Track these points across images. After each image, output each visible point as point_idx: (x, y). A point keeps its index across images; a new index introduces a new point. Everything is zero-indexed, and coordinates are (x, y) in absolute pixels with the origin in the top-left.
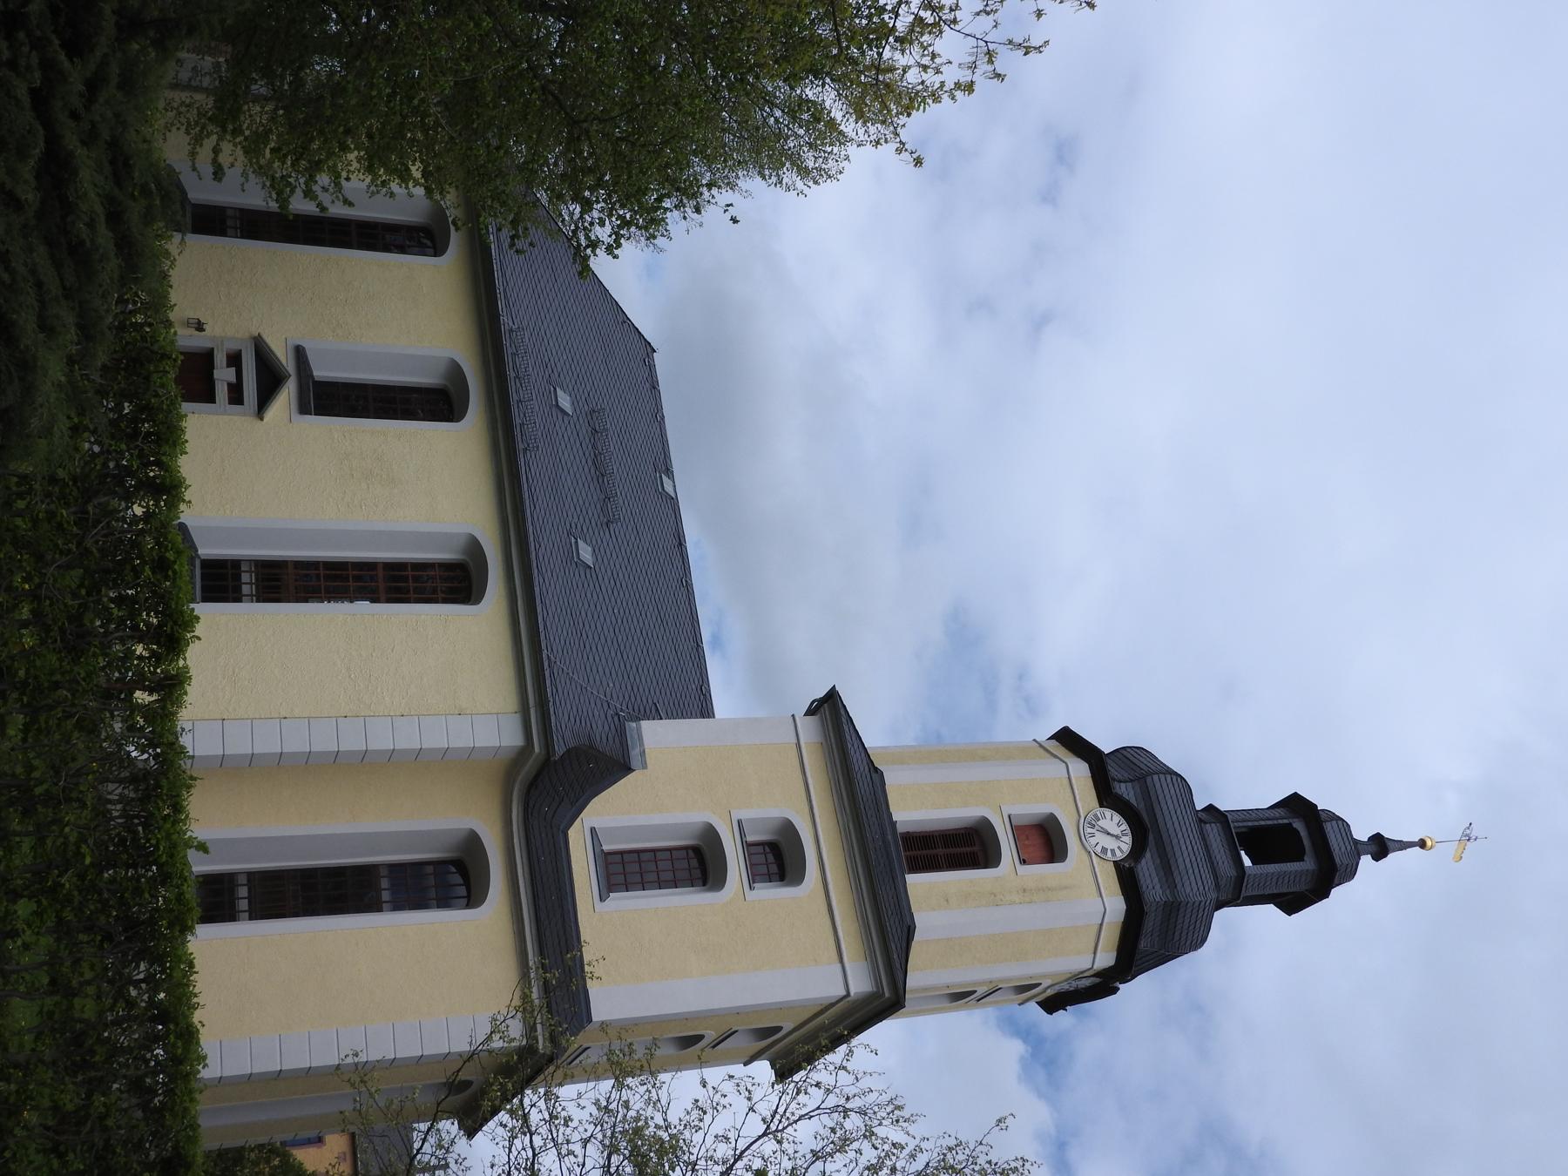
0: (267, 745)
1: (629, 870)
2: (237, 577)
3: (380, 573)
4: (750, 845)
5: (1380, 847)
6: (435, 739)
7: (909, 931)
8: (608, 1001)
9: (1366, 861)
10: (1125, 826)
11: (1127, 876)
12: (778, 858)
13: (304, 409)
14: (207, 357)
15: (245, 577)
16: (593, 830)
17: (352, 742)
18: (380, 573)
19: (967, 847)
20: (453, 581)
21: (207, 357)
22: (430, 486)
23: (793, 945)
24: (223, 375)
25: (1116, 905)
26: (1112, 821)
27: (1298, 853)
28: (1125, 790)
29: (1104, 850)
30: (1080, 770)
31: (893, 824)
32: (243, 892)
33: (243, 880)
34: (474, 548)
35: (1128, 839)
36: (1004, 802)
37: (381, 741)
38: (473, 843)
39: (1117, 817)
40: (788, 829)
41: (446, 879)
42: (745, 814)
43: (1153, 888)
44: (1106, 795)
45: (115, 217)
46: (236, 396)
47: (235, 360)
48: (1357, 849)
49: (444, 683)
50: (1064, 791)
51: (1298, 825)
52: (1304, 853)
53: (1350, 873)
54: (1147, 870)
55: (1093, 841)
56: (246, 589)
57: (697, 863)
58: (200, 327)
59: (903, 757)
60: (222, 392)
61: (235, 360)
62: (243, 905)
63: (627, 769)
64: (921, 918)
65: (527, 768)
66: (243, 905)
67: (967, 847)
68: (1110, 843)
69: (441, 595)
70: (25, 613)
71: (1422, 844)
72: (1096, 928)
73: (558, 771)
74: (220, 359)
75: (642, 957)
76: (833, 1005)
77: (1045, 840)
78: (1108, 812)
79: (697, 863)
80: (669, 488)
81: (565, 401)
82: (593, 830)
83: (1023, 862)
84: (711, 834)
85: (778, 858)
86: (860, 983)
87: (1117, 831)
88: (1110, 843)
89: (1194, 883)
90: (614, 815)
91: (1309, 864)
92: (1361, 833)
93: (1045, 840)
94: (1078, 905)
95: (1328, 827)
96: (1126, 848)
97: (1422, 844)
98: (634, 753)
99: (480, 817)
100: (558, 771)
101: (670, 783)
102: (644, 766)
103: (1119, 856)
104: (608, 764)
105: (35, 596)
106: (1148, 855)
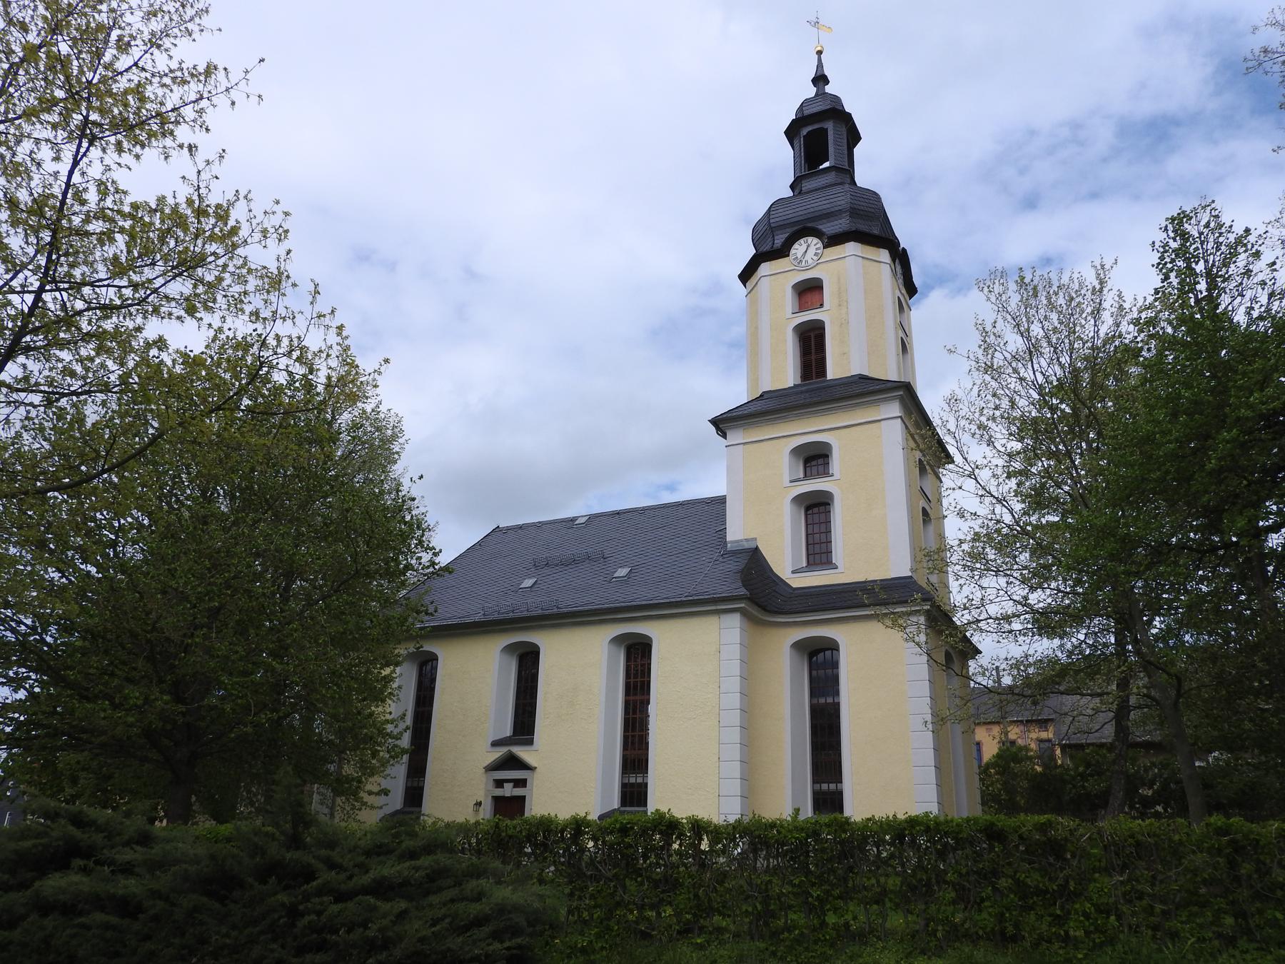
0: (735, 769)
1: (818, 550)
5: (820, 79)
6: (735, 667)
7: (863, 378)
8: (898, 565)
10: (802, 241)
11: (833, 241)
12: (814, 458)
15: (632, 780)
16: (793, 572)
17: (735, 718)
18: (631, 698)
19: (811, 341)
20: (638, 654)
22: (579, 668)
23: (868, 450)
24: (508, 790)
26: (798, 249)
27: (822, 133)
29: (816, 254)
30: (765, 268)
32: (825, 786)
35: (810, 239)
36: (784, 318)
37: (734, 700)
38: (799, 646)
39: (796, 246)
40: (796, 451)
41: (821, 664)
42: (786, 479)
44: (782, 252)
46: (521, 783)
47: (499, 783)
48: (821, 94)
49: (702, 663)
50: (779, 279)
51: (804, 132)
54: (830, 228)
55: (810, 261)
56: (640, 780)
57: (816, 509)
58: (479, 804)
59: (753, 378)
60: (518, 792)
61: (499, 783)
63: (756, 550)
64: (855, 370)
65: (755, 613)
66: (832, 786)
67: (811, 341)
68: (812, 250)
70: (651, 914)
71: (819, 53)
73: (757, 593)
74: (499, 792)
75: (872, 545)
77: (809, 291)
78: (793, 251)
79: (816, 509)
81: (528, 583)
82: (793, 572)
83: (822, 305)
84: (798, 500)
86: (894, 409)
87: (805, 246)
88: (812, 250)
89: (840, 198)
90: (785, 558)
91: (829, 126)
92: (811, 91)
93: (809, 291)
94: (850, 271)
95: (807, 112)
96: (815, 240)
97: (819, 53)
98: (747, 545)
99: (783, 642)
100: (757, 593)
103: (820, 245)
105: (641, 908)
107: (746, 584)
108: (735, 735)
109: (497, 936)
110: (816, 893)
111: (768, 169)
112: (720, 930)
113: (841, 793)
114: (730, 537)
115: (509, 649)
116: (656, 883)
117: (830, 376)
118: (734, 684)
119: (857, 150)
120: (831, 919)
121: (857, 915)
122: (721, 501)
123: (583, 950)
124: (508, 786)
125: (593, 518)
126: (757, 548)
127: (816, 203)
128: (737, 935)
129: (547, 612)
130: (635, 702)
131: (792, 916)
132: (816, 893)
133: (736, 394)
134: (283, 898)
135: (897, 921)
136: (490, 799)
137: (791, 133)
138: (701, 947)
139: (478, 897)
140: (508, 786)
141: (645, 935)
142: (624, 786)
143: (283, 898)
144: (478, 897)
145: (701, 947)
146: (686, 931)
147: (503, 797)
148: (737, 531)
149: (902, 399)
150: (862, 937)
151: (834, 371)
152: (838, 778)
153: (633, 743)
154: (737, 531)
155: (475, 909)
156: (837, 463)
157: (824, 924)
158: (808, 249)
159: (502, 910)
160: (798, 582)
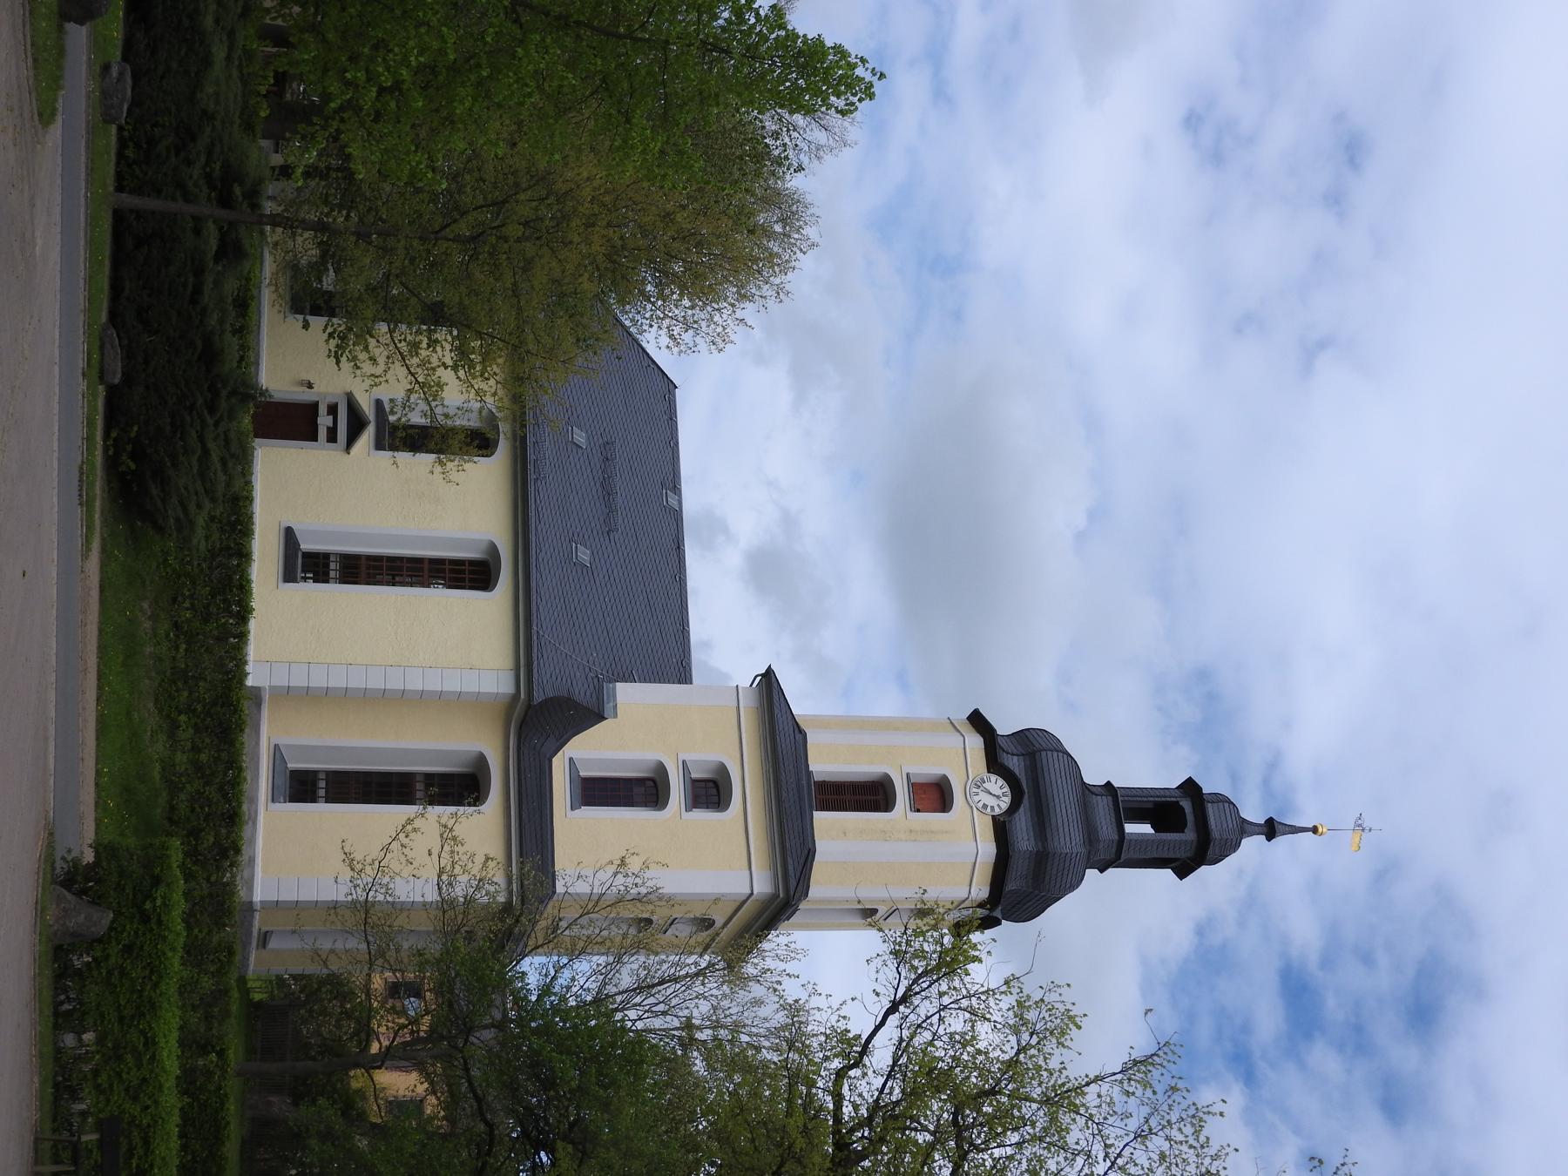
0: (338, 681)
1: (600, 791)
2: (327, 566)
3: (426, 566)
4: (694, 781)
5: (1271, 829)
6: (453, 685)
7: (810, 854)
9: (1252, 845)
10: (1007, 789)
11: (1001, 828)
12: (710, 792)
13: (379, 446)
14: (315, 405)
15: (332, 566)
16: (571, 759)
17: (395, 683)
18: (426, 566)
19: (871, 795)
20: (472, 574)
21: (315, 405)
22: (463, 505)
24: (324, 421)
25: (987, 849)
26: (997, 785)
27: (1185, 828)
28: (1014, 763)
29: (985, 806)
30: (975, 742)
31: (809, 774)
32: (322, 784)
33: (322, 776)
34: (493, 549)
35: (1008, 800)
37: (415, 683)
38: (481, 761)
39: (1001, 782)
40: (723, 770)
41: (461, 787)
42: (688, 757)
43: (1023, 838)
44: (994, 763)
45: (224, 462)
46: (332, 437)
47: (333, 410)
48: (1245, 828)
49: (460, 647)
50: (961, 760)
51: (1186, 805)
52: (1185, 825)
53: (1231, 846)
54: (1022, 827)
55: (976, 798)
56: (332, 574)
57: (645, 790)
58: (310, 386)
59: (825, 723)
60: (322, 433)
61: (333, 410)
62: (322, 793)
63: (600, 717)
64: (822, 846)
66: (322, 793)
67: (871, 795)
68: (990, 801)
69: (471, 580)
70: (187, 605)
71: (1315, 830)
72: (970, 867)
73: (545, 714)
74: (323, 409)
75: (589, 847)
76: (744, 902)
77: (935, 795)
78: (993, 777)
79: (645, 790)
80: (673, 501)
81: (580, 437)
82: (571, 759)
84: (661, 770)
85: (710, 792)
86: (763, 885)
87: (999, 792)
88: (990, 801)
89: (1068, 838)
90: (591, 750)
91: (1189, 835)
92: (1253, 812)
93: (935, 795)
95: (1211, 810)
96: (1005, 806)
97: (1315, 830)
98: (608, 707)
99: (483, 741)
100: (545, 714)
101: (639, 726)
102: (615, 716)
103: (997, 811)
104: (592, 714)
105: (191, 597)
106: (1022, 809)
107: (550, 703)
108: (375, 682)
109: (178, 520)
110: (199, 708)
111: (1121, 751)
112: (177, 648)
113: (314, 800)
114: (621, 687)
115: (492, 420)
116: (207, 607)
117: (816, 814)
118: (433, 684)
119: (1168, 874)
120: (183, 718)
121: (186, 734)
122: (683, 675)
123: (166, 560)
124: (328, 421)
125: (677, 516)
126: (604, 719)
127: (1064, 808)
128: (174, 658)
129: (530, 467)
130: (422, 569)
131: (185, 694)
132: (199, 708)
133: (802, 701)
134: (200, 401)
135: (180, 758)
136: (315, 398)
137: (1190, 787)
138: (167, 635)
139: (199, 506)
140: (328, 421)
141: (174, 600)
142: (326, 556)
143: (200, 401)
144: (199, 506)
145: (167, 635)
146: (176, 626)
147: (316, 415)
148: (628, 695)
149: (775, 896)
150: (172, 735)
151: (823, 820)
152: (332, 798)
153: (375, 568)
154: (628, 695)
155: (192, 507)
156: (702, 816)
157: (180, 713)
158: (996, 794)
159: (192, 523)
160: (559, 765)
